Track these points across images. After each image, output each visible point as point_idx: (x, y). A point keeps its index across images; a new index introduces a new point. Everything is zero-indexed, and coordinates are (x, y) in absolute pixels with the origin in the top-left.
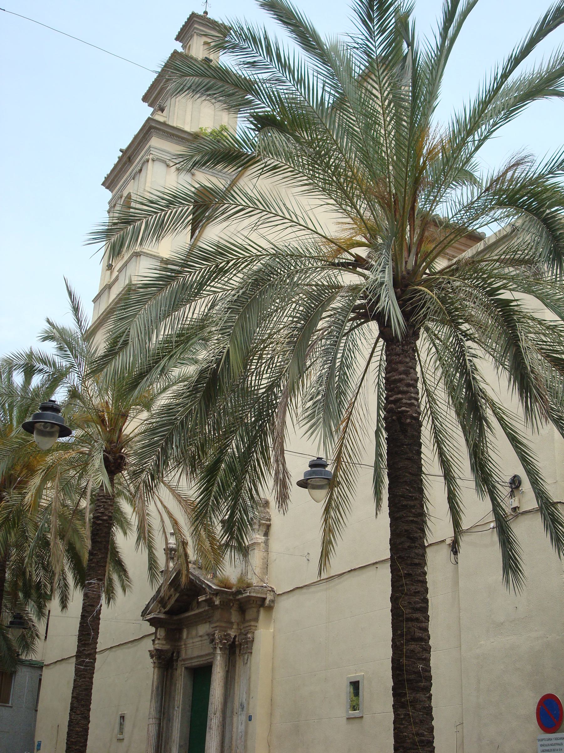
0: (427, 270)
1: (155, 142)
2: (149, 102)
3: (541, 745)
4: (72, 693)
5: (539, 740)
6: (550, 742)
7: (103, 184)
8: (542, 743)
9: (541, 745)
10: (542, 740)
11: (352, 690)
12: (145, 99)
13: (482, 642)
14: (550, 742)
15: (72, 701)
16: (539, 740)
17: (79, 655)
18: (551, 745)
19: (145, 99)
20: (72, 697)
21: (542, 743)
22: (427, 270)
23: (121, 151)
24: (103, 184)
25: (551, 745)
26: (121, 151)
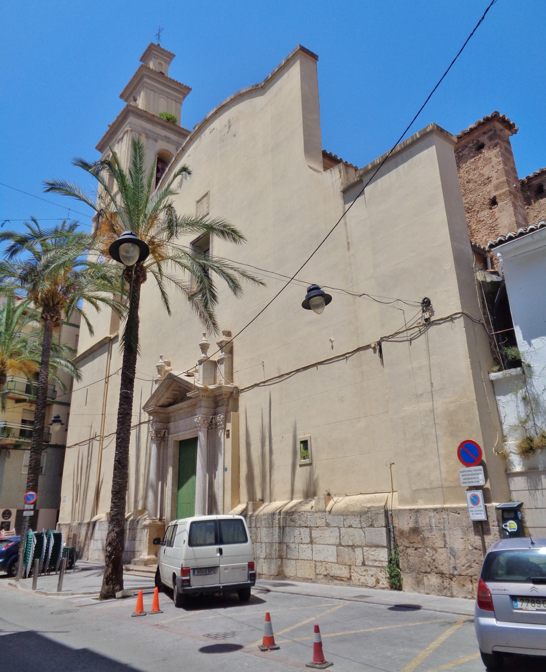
0: (500, 255)
1: (131, 119)
2: (125, 98)
3: (463, 475)
4: (115, 458)
5: (461, 472)
6: (470, 473)
7: (97, 148)
8: (463, 474)
9: (463, 475)
10: (463, 472)
11: (356, 509)
12: (122, 96)
13: (406, 408)
14: (470, 473)
15: (115, 464)
16: (461, 472)
17: (118, 433)
18: (471, 475)
19: (122, 96)
20: (115, 461)
21: (463, 474)
22: (500, 255)
23: (109, 126)
24: (97, 148)
25: (471, 475)
26: (109, 126)
